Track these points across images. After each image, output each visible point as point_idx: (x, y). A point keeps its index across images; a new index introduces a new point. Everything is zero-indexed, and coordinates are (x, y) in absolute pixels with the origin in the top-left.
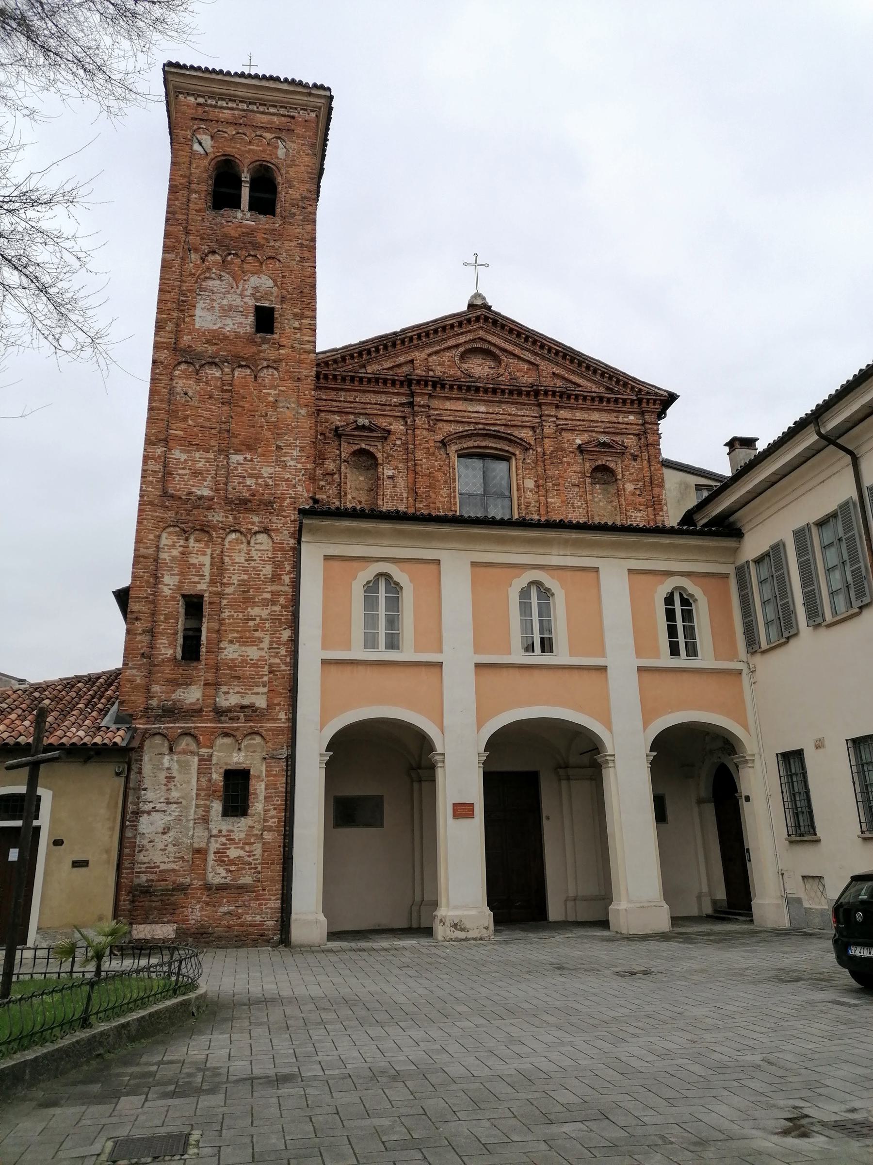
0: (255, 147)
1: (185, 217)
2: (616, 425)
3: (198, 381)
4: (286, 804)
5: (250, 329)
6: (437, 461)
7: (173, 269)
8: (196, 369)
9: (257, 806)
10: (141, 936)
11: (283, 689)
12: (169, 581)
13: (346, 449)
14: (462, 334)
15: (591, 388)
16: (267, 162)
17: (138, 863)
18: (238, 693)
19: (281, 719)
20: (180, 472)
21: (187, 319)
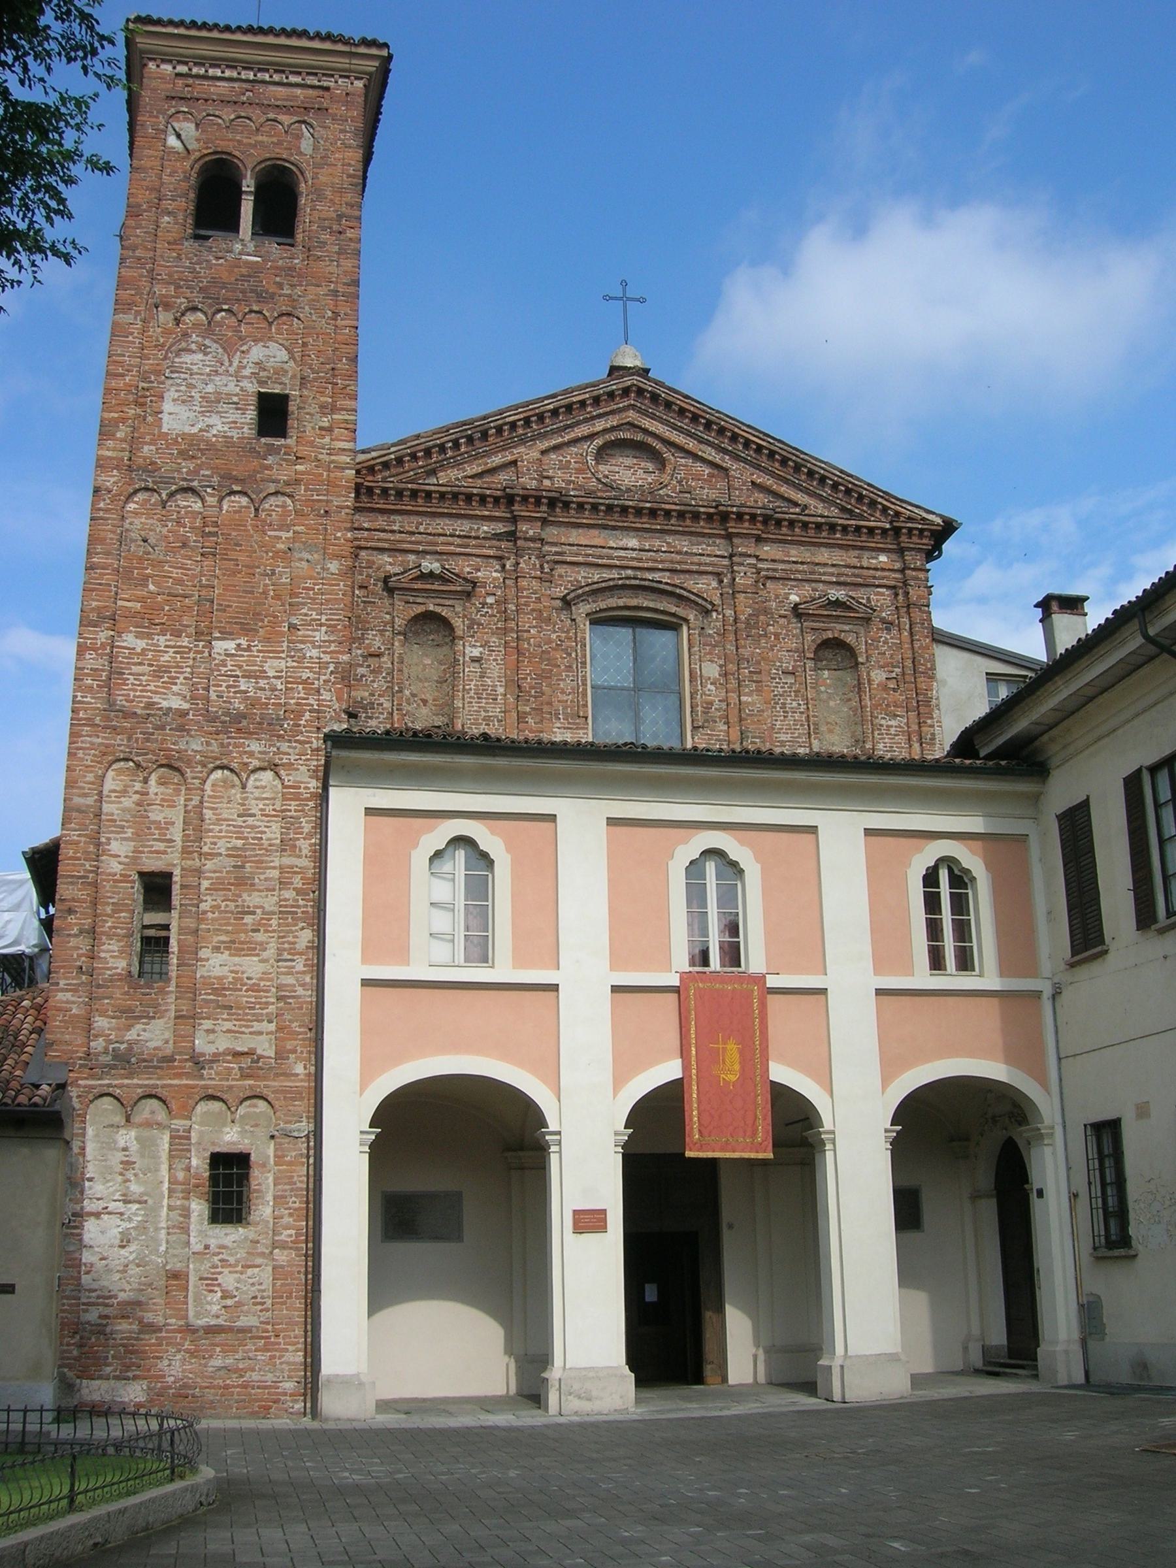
0: (265, 139)
1: (151, 254)
2: (857, 571)
3: (163, 521)
4: (307, 1209)
5: (249, 431)
6: (555, 632)
7: (130, 338)
8: (162, 501)
9: (263, 1209)
10: (96, 1397)
11: (300, 1026)
12: (119, 848)
13: (403, 612)
14: (600, 416)
15: (815, 507)
16: (284, 160)
17: (86, 1290)
18: (229, 1031)
19: (297, 1075)
20: (135, 669)
21: (150, 419)
